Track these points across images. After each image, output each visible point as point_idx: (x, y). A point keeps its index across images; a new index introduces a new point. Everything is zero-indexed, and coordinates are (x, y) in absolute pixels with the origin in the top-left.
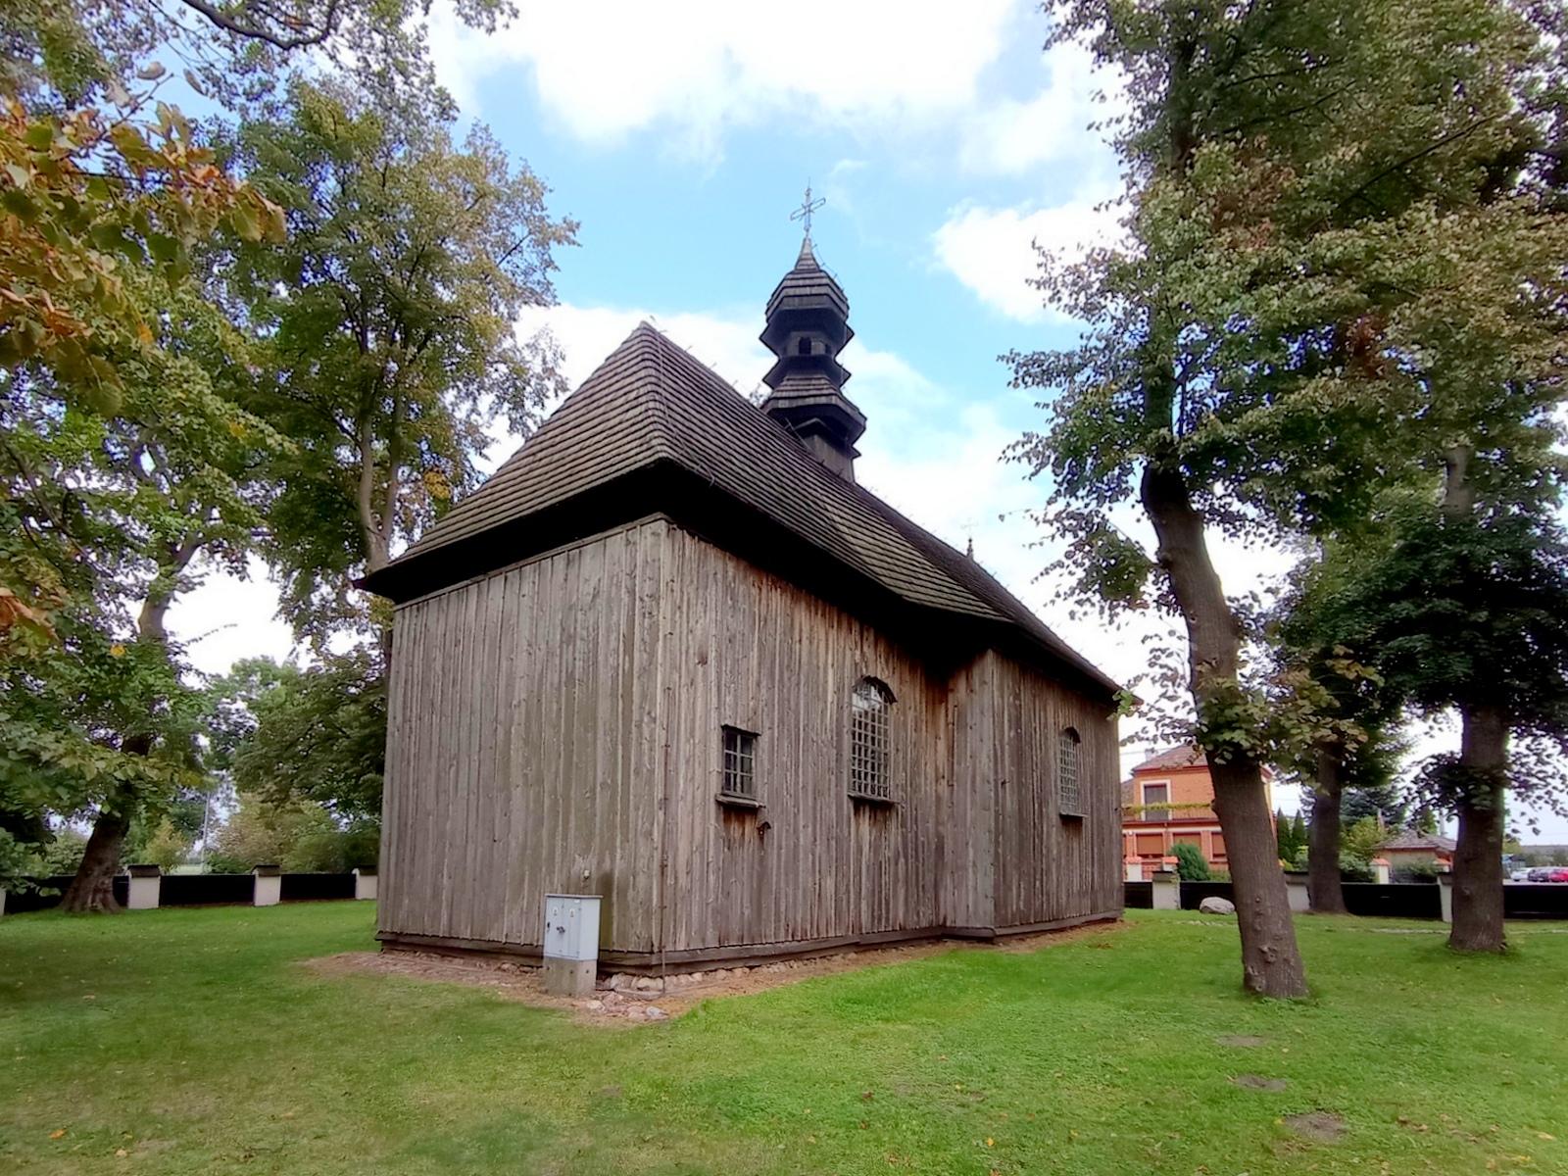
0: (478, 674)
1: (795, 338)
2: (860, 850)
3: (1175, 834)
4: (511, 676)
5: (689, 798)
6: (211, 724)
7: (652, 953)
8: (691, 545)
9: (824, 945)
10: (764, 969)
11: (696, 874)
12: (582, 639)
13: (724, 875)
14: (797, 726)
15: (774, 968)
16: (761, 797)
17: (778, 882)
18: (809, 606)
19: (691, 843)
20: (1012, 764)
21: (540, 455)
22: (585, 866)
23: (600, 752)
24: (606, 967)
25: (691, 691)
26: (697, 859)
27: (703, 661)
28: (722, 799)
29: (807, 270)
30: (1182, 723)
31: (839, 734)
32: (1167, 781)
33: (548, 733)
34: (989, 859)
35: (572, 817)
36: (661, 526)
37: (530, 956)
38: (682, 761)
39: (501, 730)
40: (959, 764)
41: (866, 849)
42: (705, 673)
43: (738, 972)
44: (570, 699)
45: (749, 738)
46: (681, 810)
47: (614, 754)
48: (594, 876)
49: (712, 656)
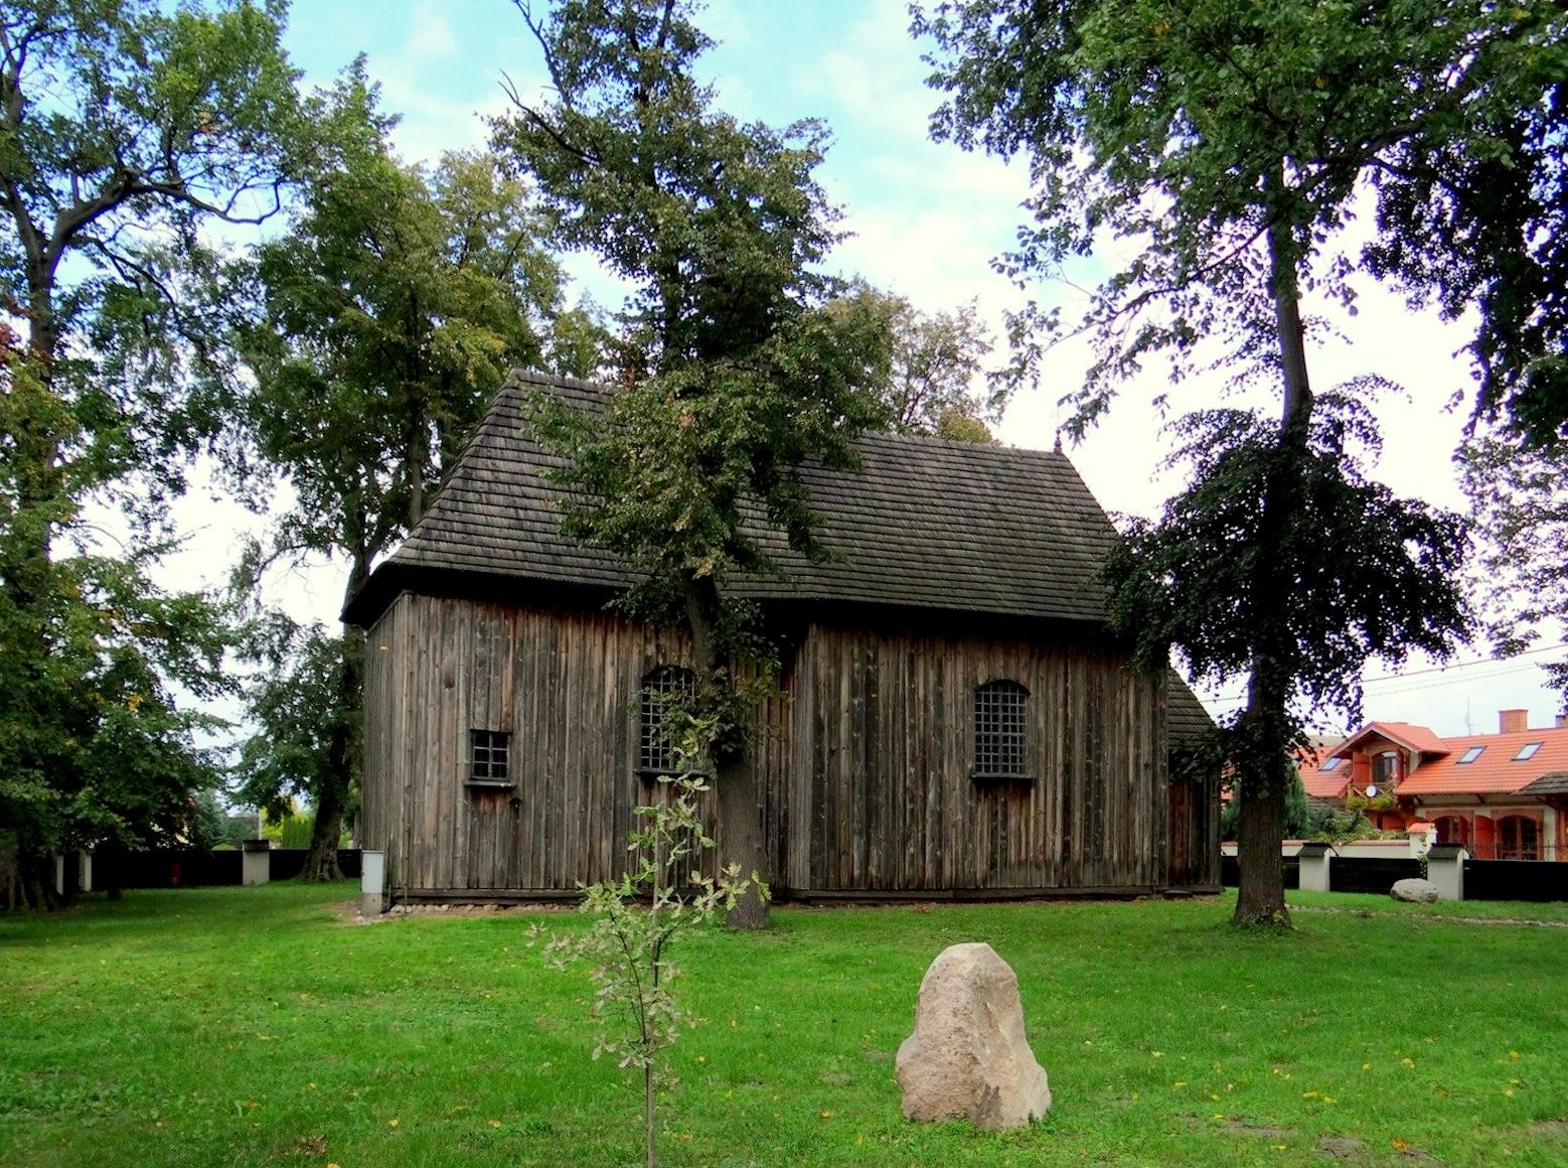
13: (473, 838)
19: (438, 816)
20: (855, 726)
26: (443, 827)
27: (450, 684)
30: (1089, 681)
31: (622, 723)
42: (451, 696)
45: (502, 738)
46: (429, 797)
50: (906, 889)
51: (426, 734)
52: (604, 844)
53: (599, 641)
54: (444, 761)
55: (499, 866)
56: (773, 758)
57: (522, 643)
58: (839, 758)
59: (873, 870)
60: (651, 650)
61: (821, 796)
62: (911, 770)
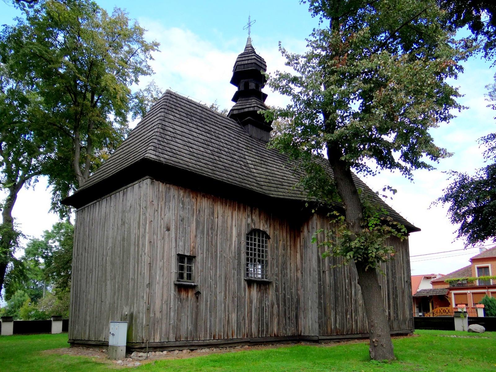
0: (98, 237)
1: (243, 82)
2: (251, 302)
3: (473, 293)
4: (107, 238)
5: (161, 283)
6: (44, 253)
7: (143, 343)
8: (162, 187)
9: (229, 342)
10: (199, 351)
11: (164, 312)
12: (127, 223)
13: (178, 312)
14: (216, 252)
15: (204, 350)
16: (197, 280)
17: (206, 315)
18: (222, 203)
19: (162, 300)
21: (125, 149)
22: (126, 311)
23: (131, 266)
24: (130, 349)
25: (162, 241)
26: (164, 306)
27: (168, 229)
28: (178, 283)
29: (250, 51)
31: (239, 254)
32: (489, 264)
33: (117, 260)
34: (316, 305)
35: (123, 292)
36: (149, 181)
37: (103, 345)
38: (158, 269)
39: (104, 259)
40: (305, 263)
41: (255, 301)
42: (169, 235)
43: (185, 351)
44: (123, 244)
45: (191, 258)
46: (157, 289)
47: (134, 267)
48: (129, 314)
49: (173, 228)
50: (347, 334)
51: (157, 254)
52: (233, 315)
53: (230, 214)
54: (165, 270)
55: (190, 328)
56: (292, 275)
57: (199, 211)
58: (325, 274)
59: (337, 326)
60: (249, 220)
61: (321, 292)
62: (347, 281)
